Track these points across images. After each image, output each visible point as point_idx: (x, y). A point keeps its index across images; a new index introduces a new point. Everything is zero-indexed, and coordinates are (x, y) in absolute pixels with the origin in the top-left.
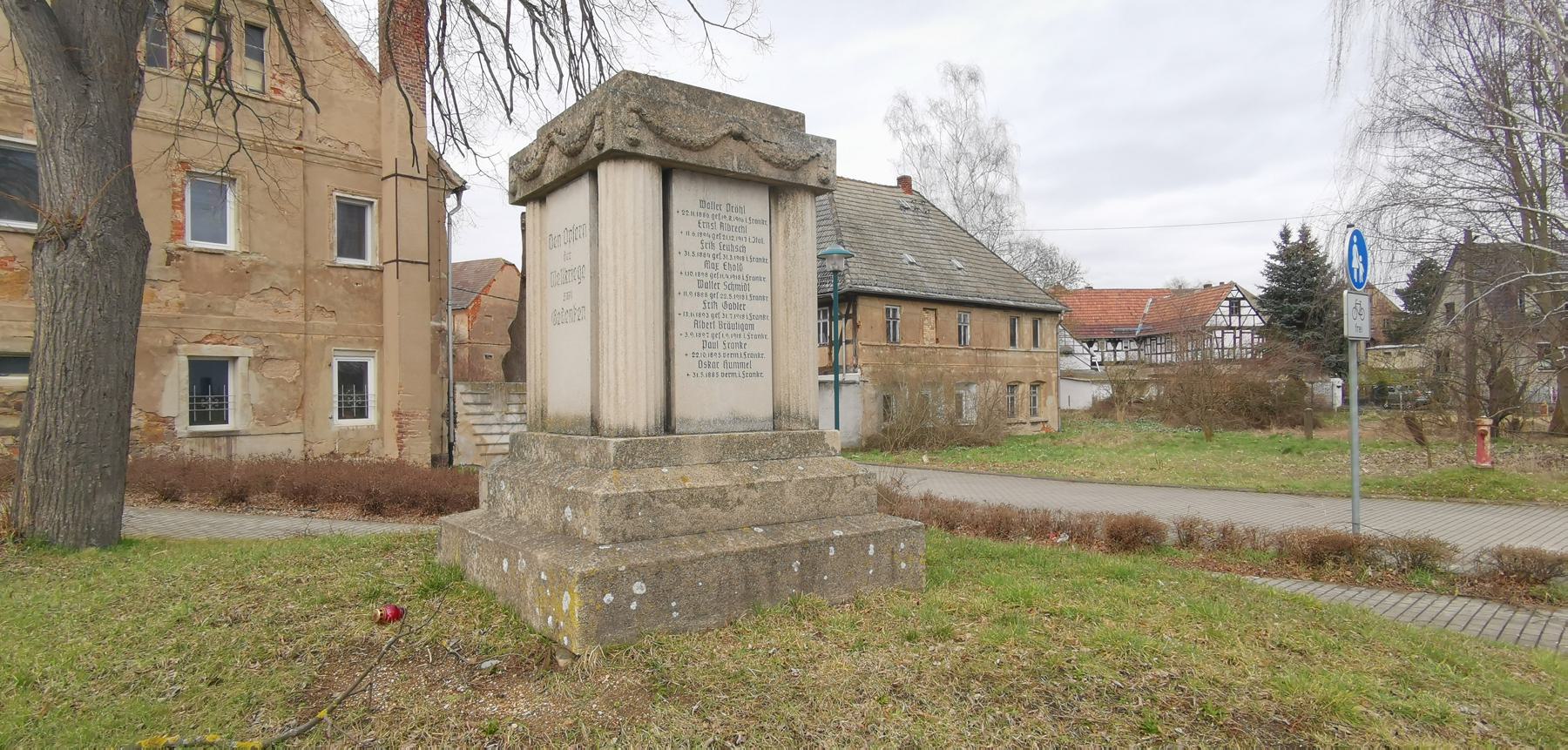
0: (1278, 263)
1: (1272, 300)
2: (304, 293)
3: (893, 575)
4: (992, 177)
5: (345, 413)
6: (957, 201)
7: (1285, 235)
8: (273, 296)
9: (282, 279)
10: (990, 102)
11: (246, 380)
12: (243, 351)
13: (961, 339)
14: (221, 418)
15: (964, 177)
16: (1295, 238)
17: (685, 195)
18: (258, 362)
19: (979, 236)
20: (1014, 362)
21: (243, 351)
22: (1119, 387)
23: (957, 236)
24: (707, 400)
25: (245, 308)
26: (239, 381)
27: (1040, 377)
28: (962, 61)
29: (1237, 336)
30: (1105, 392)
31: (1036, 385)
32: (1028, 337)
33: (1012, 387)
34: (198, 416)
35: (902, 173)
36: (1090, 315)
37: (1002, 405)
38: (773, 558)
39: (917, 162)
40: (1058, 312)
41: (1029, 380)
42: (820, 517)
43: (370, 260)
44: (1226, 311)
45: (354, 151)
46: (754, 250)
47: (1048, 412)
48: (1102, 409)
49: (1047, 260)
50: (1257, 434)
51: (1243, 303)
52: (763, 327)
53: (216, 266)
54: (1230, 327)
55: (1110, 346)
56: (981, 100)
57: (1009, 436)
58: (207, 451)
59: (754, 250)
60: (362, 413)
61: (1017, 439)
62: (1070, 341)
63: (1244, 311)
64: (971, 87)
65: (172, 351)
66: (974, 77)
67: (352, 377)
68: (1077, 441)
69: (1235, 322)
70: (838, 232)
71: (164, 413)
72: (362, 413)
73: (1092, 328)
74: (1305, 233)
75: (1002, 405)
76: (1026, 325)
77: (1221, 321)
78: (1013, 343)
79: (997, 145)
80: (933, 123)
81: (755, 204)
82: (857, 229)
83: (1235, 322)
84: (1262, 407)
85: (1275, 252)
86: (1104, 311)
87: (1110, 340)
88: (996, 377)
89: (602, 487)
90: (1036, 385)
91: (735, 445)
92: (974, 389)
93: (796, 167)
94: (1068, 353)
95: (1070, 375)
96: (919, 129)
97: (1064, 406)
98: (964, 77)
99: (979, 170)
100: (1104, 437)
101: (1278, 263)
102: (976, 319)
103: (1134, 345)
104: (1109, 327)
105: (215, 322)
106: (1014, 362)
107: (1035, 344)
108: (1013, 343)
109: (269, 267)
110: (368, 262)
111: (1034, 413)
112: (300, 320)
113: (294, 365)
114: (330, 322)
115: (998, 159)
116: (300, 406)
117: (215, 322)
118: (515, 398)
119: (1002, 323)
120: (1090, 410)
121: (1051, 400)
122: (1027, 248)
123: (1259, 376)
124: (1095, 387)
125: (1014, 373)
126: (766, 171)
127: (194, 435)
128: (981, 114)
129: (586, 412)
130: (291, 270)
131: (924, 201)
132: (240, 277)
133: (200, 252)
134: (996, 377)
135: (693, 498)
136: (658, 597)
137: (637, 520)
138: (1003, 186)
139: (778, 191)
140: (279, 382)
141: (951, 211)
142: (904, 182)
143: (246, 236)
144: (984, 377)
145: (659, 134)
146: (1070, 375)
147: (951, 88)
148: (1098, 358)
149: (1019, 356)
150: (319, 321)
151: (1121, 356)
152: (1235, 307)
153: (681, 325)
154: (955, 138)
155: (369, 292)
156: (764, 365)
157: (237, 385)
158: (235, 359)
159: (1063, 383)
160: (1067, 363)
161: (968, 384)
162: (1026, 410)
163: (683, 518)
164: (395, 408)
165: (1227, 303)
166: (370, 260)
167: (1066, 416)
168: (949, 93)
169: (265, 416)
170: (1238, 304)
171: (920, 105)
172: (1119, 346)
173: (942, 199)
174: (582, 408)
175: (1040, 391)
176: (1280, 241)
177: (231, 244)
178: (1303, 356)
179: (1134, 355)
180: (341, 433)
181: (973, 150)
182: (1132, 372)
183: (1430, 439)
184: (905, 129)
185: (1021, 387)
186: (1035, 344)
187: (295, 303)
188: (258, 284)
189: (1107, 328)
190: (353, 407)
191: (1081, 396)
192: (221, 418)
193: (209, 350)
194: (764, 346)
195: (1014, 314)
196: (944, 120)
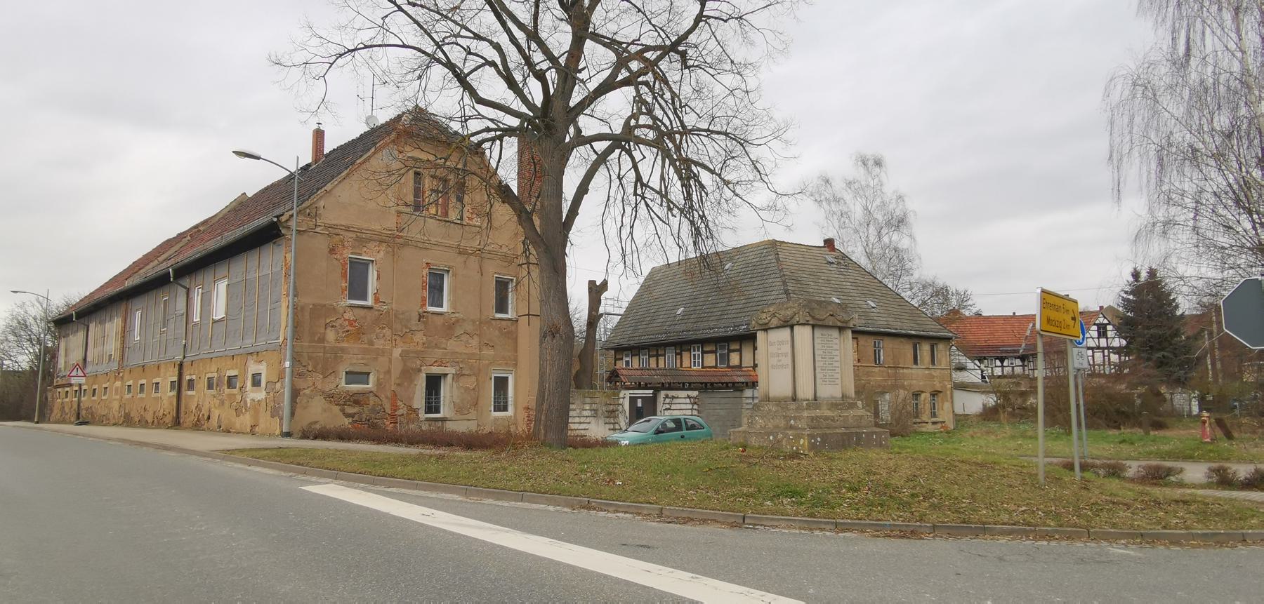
0: (1131, 297)
1: (1126, 326)
2: (479, 336)
3: (881, 445)
4: (895, 237)
5: (497, 409)
6: (869, 255)
7: (1136, 275)
8: (465, 337)
9: (469, 327)
10: (894, 181)
11: (452, 387)
12: (450, 371)
13: (876, 359)
14: (438, 411)
15: (873, 238)
16: (1144, 275)
17: (818, 332)
18: (457, 377)
19: (885, 281)
20: (917, 376)
21: (450, 371)
22: (1004, 395)
23: (869, 282)
24: (826, 391)
25: (452, 345)
26: (448, 388)
27: (938, 387)
28: (870, 152)
29: (1093, 354)
30: (991, 400)
31: (934, 394)
32: (927, 358)
33: (917, 395)
34: (429, 409)
35: (829, 235)
36: (980, 337)
37: (909, 409)
38: (850, 435)
39: (836, 225)
40: (948, 339)
41: (929, 390)
42: (859, 427)
43: (511, 314)
44: (1095, 334)
45: (505, 250)
46: (835, 347)
47: (945, 415)
48: (989, 414)
49: (942, 293)
50: (1112, 432)
51: (1110, 328)
52: (838, 370)
53: (439, 320)
54: (1098, 348)
55: (998, 363)
56: (884, 180)
57: (916, 432)
58: (435, 427)
59: (835, 347)
60: (505, 409)
61: (921, 433)
62: (963, 359)
63: (1110, 334)
64: (877, 170)
65: (420, 370)
66: (878, 163)
67: (501, 384)
68: (967, 435)
69: (1103, 342)
70: (784, 283)
71: (415, 406)
72: (505, 409)
73: (982, 348)
74: (1152, 273)
75: (909, 409)
76: (925, 348)
77: (1091, 343)
78: (915, 362)
79: (898, 212)
80: (848, 197)
81: (835, 333)
82: (798, 281)
83: (1103, 342)
84: (1118, 412)
85: (1128, 289)
86: (991, 334)
87: (997, 358)
88: (904, 388)
89: (805, 414)
90: (934, 394)
91: (834, 405)
92: (887, 396)
93: (846, 322)
94: (961, 368)
95: (963, 387)
96: (837, 200)
97: (959, 411)
98: (870, 163)
99: (884, 231)
100: (988, 433)
101: (1131, 297)
102: (887, 345)
103: (1018, 362)
104: (997, 347)
105: (438, 353)
106: (917, 376)
107: (933, 362)
108: (915, 362)
109: (464, 320)
110: (509, 316)
111: (934, 415)
112: (477, 351)
113: (474, 379)
114: (492, 352)
115: (899, 223)
116: (475, 404)
117: (438, 353)
118: (588, 400)
119: (907, 348)
120: (981, 415)
121: (947, 405)
122: (924, 287)
123: (1122, 387)
124: (983, 397)
125: (917, 384)
126: (839, 324)
127: (428, 419)
128: (885, 189)
129: (789, 393)
130: (474, 322)
131: (844, 257)
132: (450, 327)
133: (434, 313)
134: (904, 388)
135: (826, 418)
136: (823, 442)
137: (815, 423)
138: (905, 243)
139: (841, 329)
140: (467, 389)
141: (863, 262)
142: (829, 243)
143: (453, 304)
144: (895, 387)
145: (813, 318)
146: (963, 387)
147: (862, 170)
148: (987, 372)
149: (920, 372)
150: (488, 352)
151: (1008, 370)
152: (1102, 332)
153: (818, 370)
154: (866, 209)
155: (510, 333)
156: (839, 382)
157: (446, 390)
158: (446, 375)
159: (957, 394)
160: (959, 377)
161: (883, 393)
162: (928, 412)
163: (824, 423)
164: (526, 404)
165: (1095, 328)
166: (511, 314)
167: (962, 420)
168: (859, 174)
169: (459, 409)
170: (1105, 328)
171: (838, 185)
172: (1005, 364)
173: (857, 253)
174: (788, 392)
175: (938, 399)
176: (1131, 279)
177: (445, 309)
178: (1151, 371)
179: (1018, 370)
180: (496, 419)
181: (879, 216)
182: (1018, 384)
183: (1236, 435)
184: (827, 200)
185: (923, 395)
186: (933, 362)
187: (475, 342)
188: (459, 331)
189: (995, 348)
190: (501, 406)
191: (974, 403)
192: (438, 411)
193: (436, 370)
194: (839, 376)
195: (916, 341)
196: (856, 194)
